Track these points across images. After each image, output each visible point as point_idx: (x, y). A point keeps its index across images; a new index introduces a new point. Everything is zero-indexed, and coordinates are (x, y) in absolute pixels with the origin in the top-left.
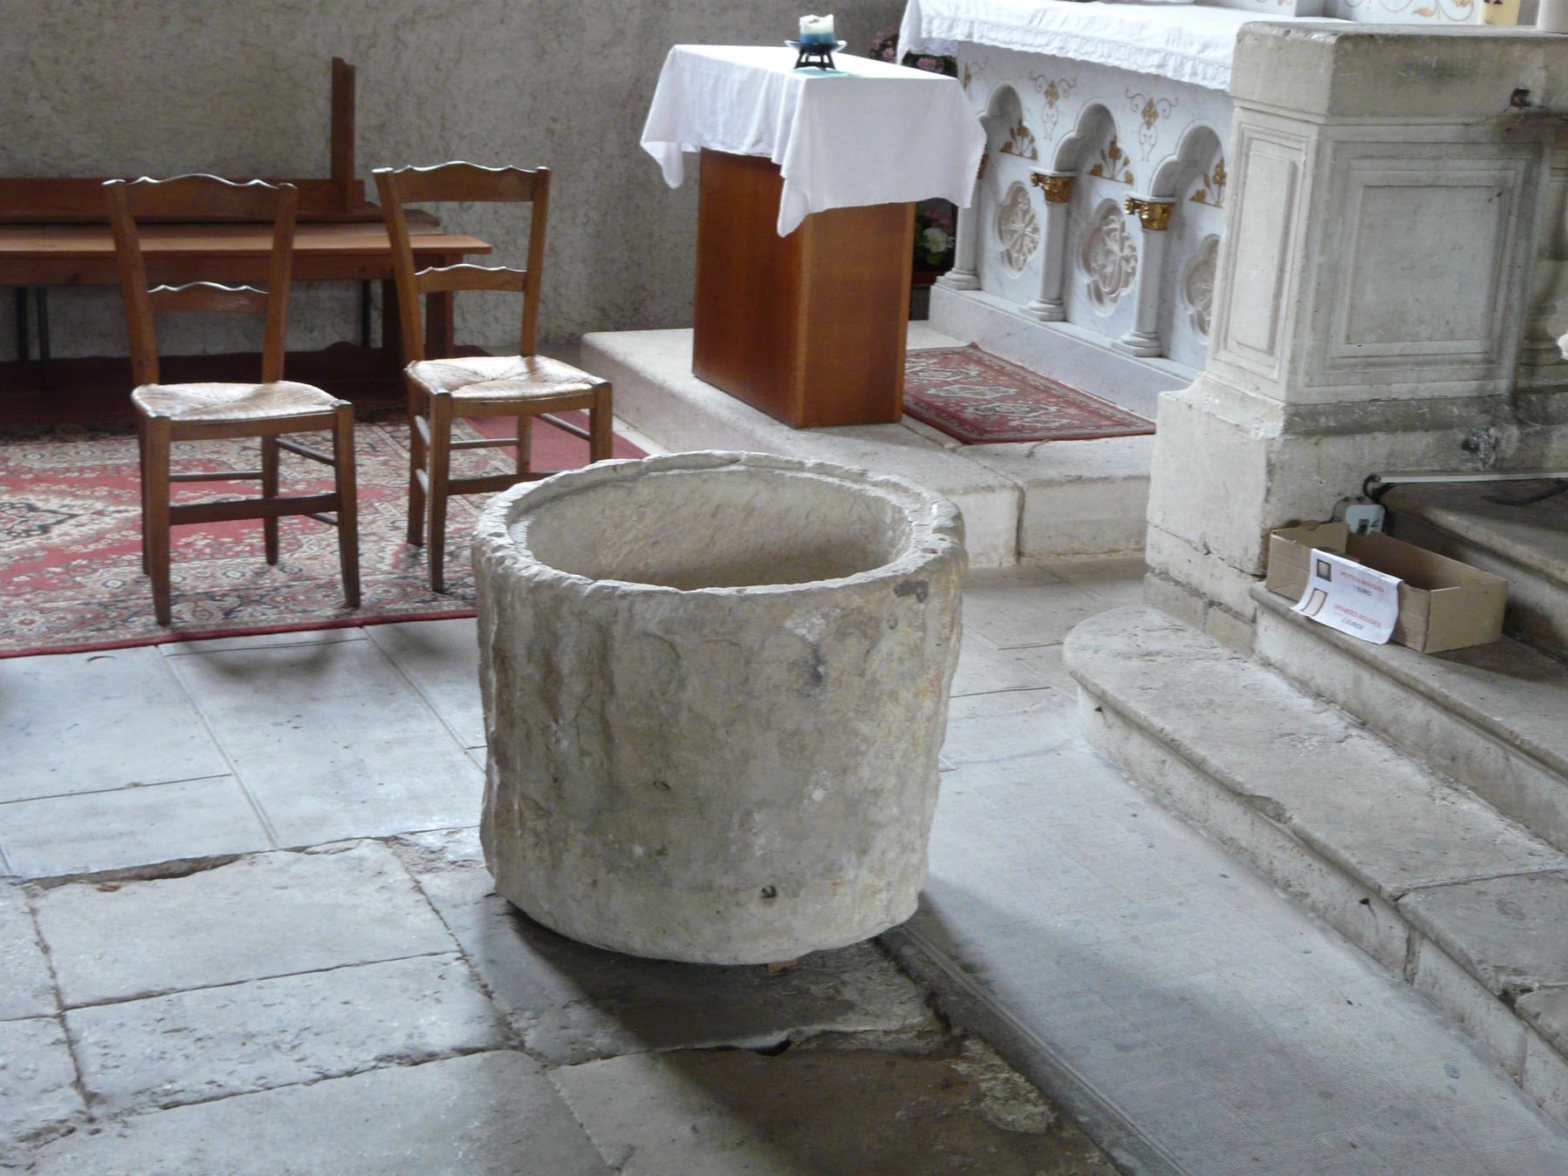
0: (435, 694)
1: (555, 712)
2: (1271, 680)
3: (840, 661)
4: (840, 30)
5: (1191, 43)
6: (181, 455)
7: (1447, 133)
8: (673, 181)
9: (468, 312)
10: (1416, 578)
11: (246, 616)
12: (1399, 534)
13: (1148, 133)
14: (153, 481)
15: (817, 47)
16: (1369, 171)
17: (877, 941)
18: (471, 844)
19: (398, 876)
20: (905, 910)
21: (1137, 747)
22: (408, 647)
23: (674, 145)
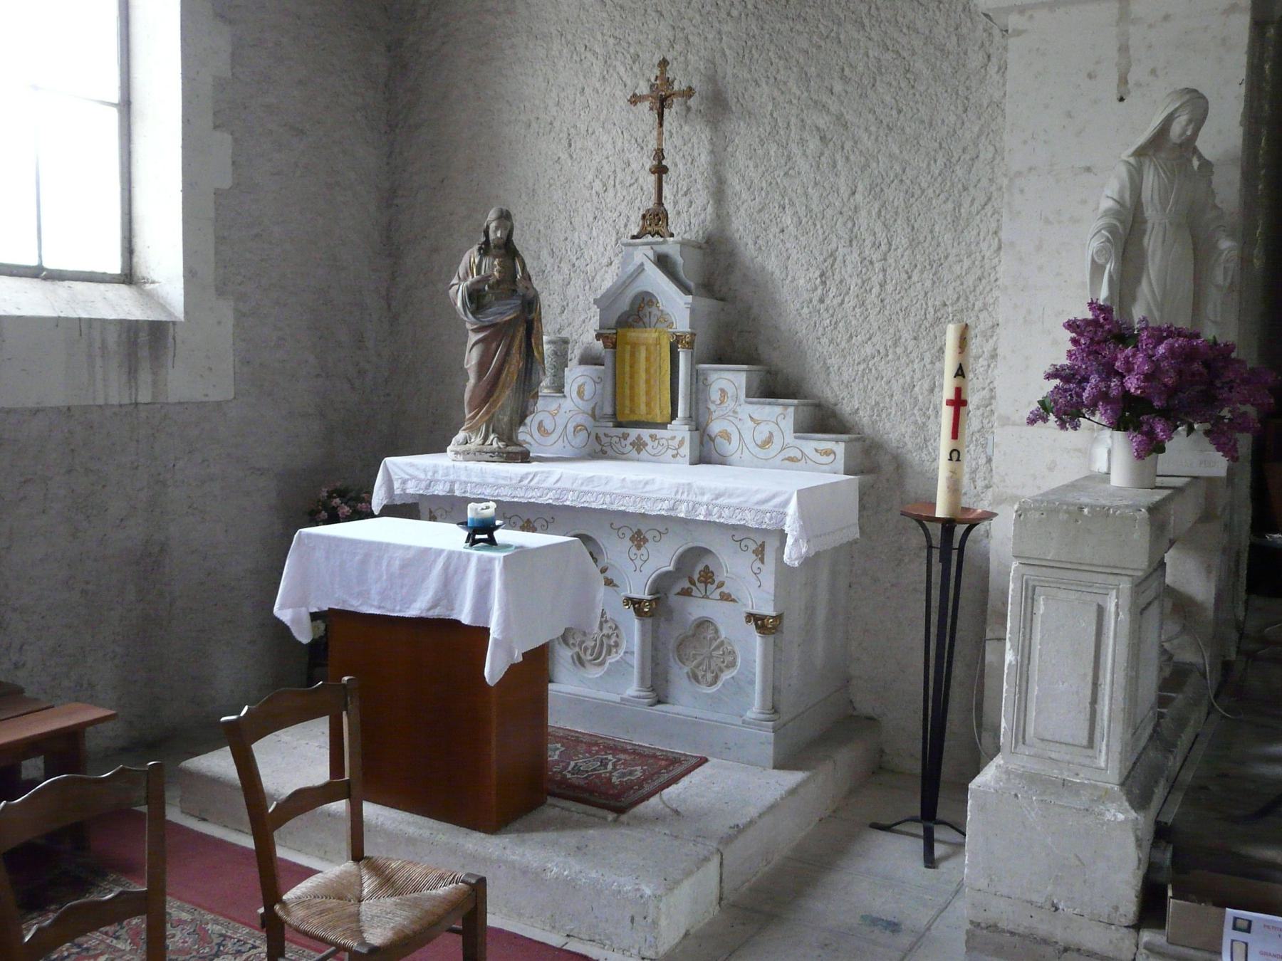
5: (703, 494)
13: (639, 553)
23: (304, 609)
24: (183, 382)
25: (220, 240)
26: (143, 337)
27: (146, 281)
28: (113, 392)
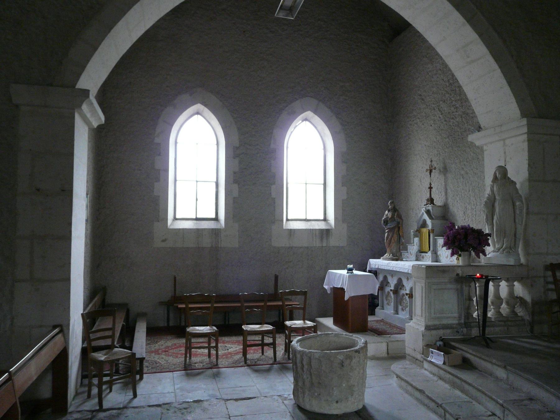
0: (287, 375)
1: (303, 371)
2: (426, 372)
3: (347, 362)
4: (354, 267)
6: (249, 338)
7: (447, 281)
8: (329, 292)
9: (296, 312)
10: (446, 353)
11: (258, 363)
12: (445, 347)
14: (245, 341)
15: (351, 270)
16: (435, 287)
17: (356, 412)
18: (292, 397)
19: (280, 401)
20: (360, 407)
21: (403, 383)
22: (283, 368)
24: (334, 242)
25: (343, 210)
26: (325, 232)
27: (328, 220)
28: (317, 243)
